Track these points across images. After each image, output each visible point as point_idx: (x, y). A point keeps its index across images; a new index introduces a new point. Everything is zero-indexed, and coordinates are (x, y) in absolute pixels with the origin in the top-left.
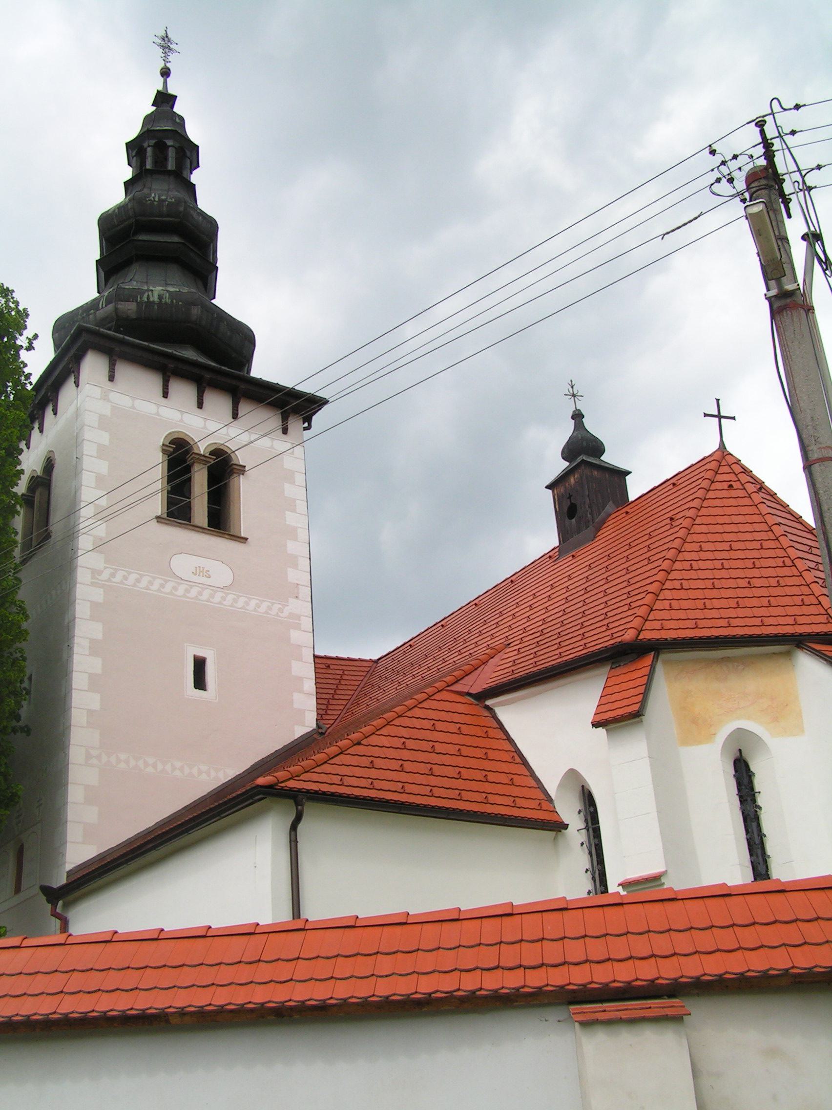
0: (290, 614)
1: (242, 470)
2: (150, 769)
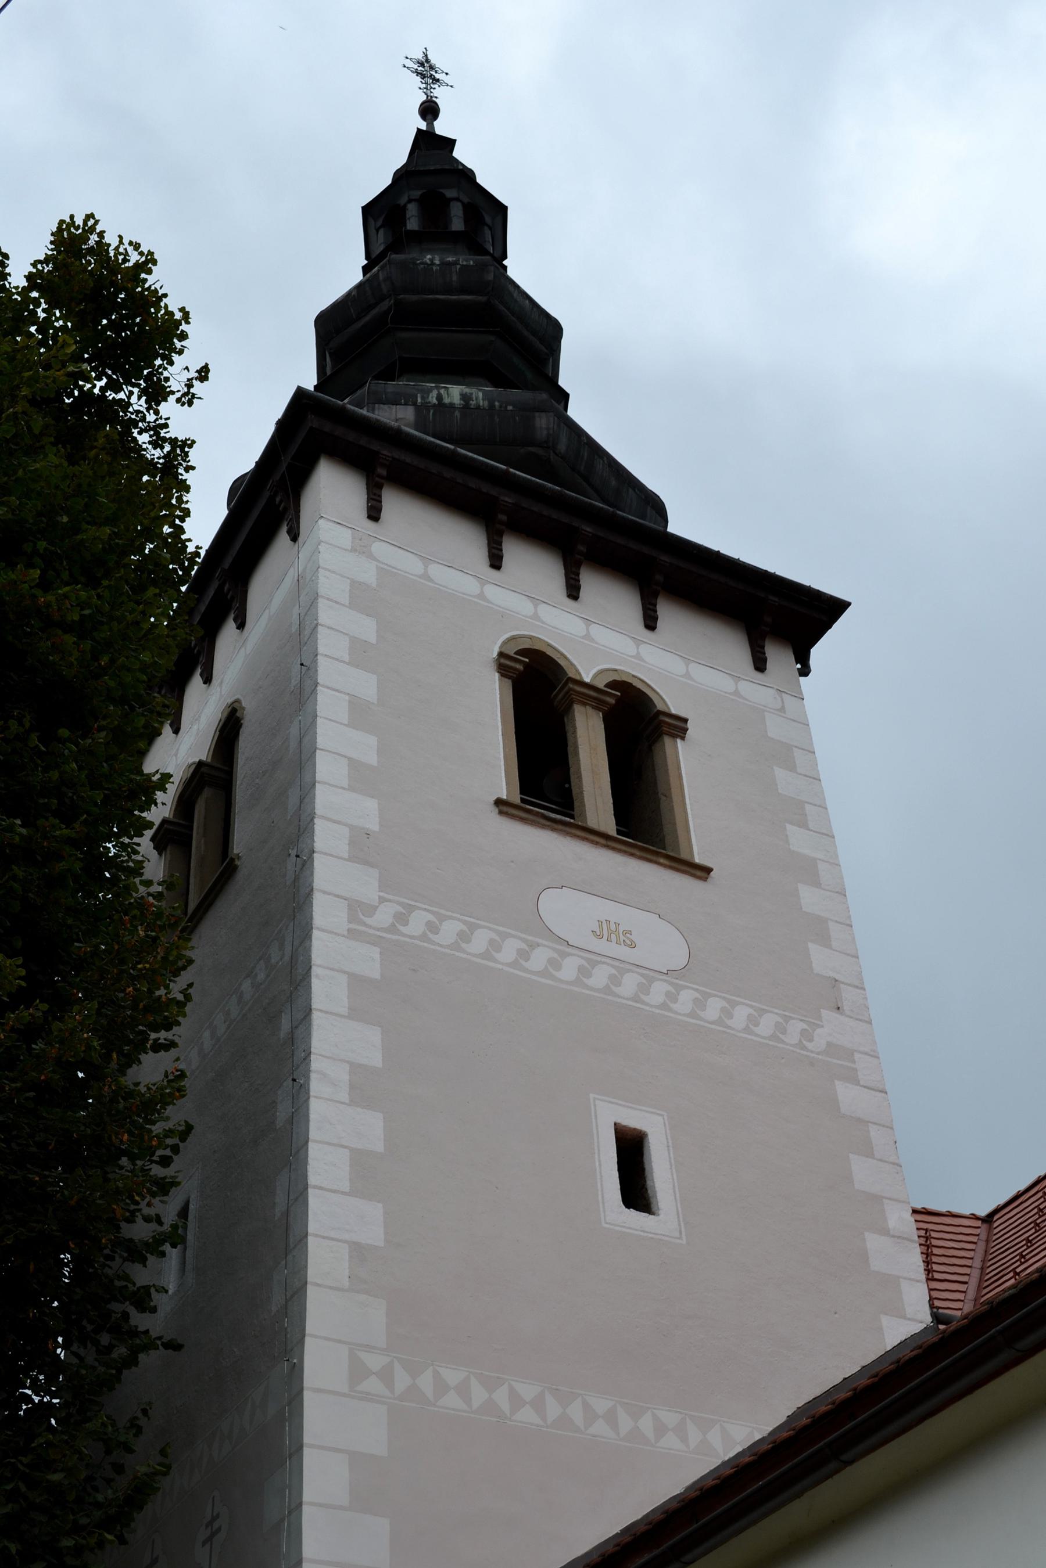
0: (829, 1044)
1: (679, 727)
2: (527, 1415)
